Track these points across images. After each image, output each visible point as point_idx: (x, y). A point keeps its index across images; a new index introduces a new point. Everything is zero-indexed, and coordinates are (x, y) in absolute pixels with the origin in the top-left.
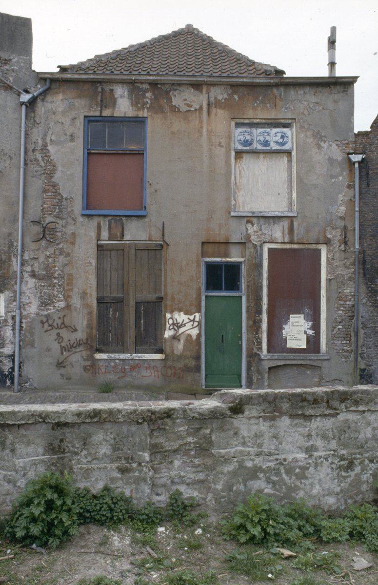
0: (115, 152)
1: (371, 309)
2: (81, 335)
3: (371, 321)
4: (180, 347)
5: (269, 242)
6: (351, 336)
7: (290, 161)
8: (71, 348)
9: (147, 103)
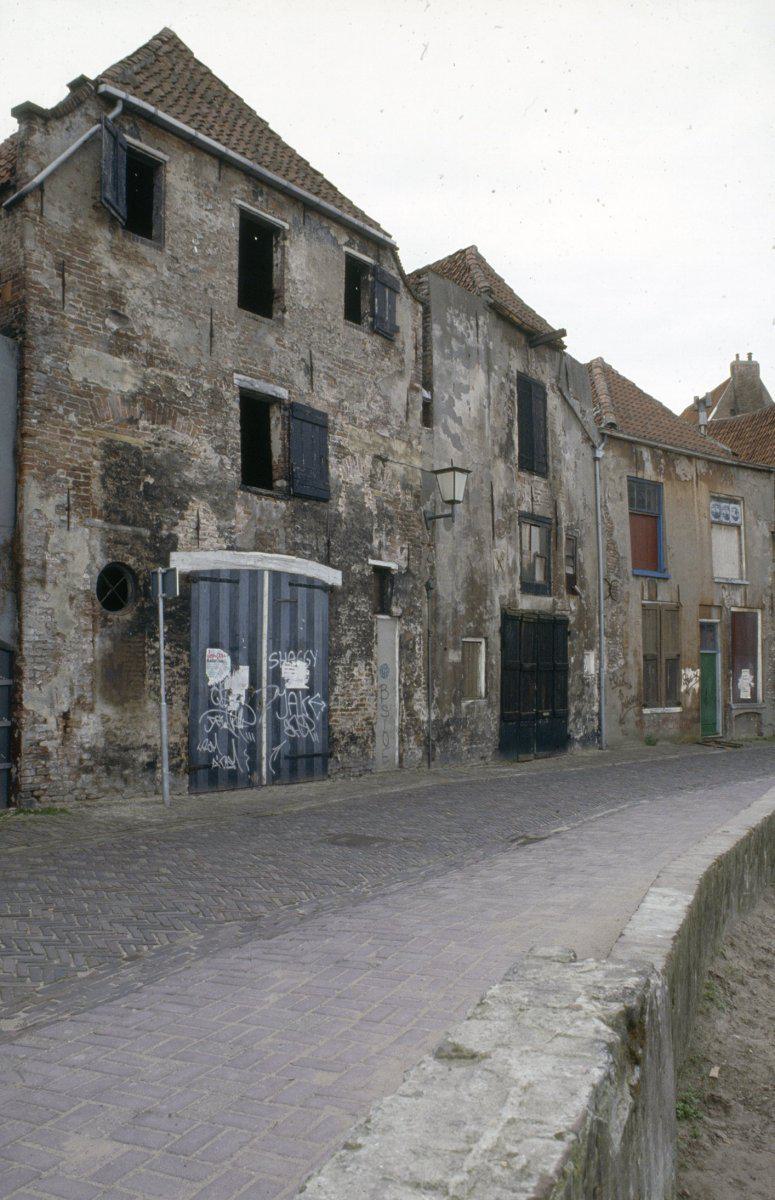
2: (633, 692)
7: (740, 534)
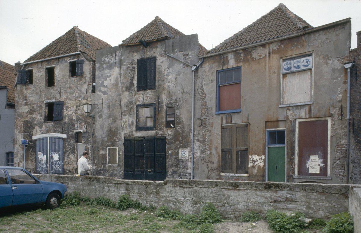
0: (229, 84)
1: (357, 152)
2: (215, 165)
3: (357, 159)
4: (255, 171)
5: (298, 119)
6: (345, 167)
8: (211, 171)
9: (242, 59)
